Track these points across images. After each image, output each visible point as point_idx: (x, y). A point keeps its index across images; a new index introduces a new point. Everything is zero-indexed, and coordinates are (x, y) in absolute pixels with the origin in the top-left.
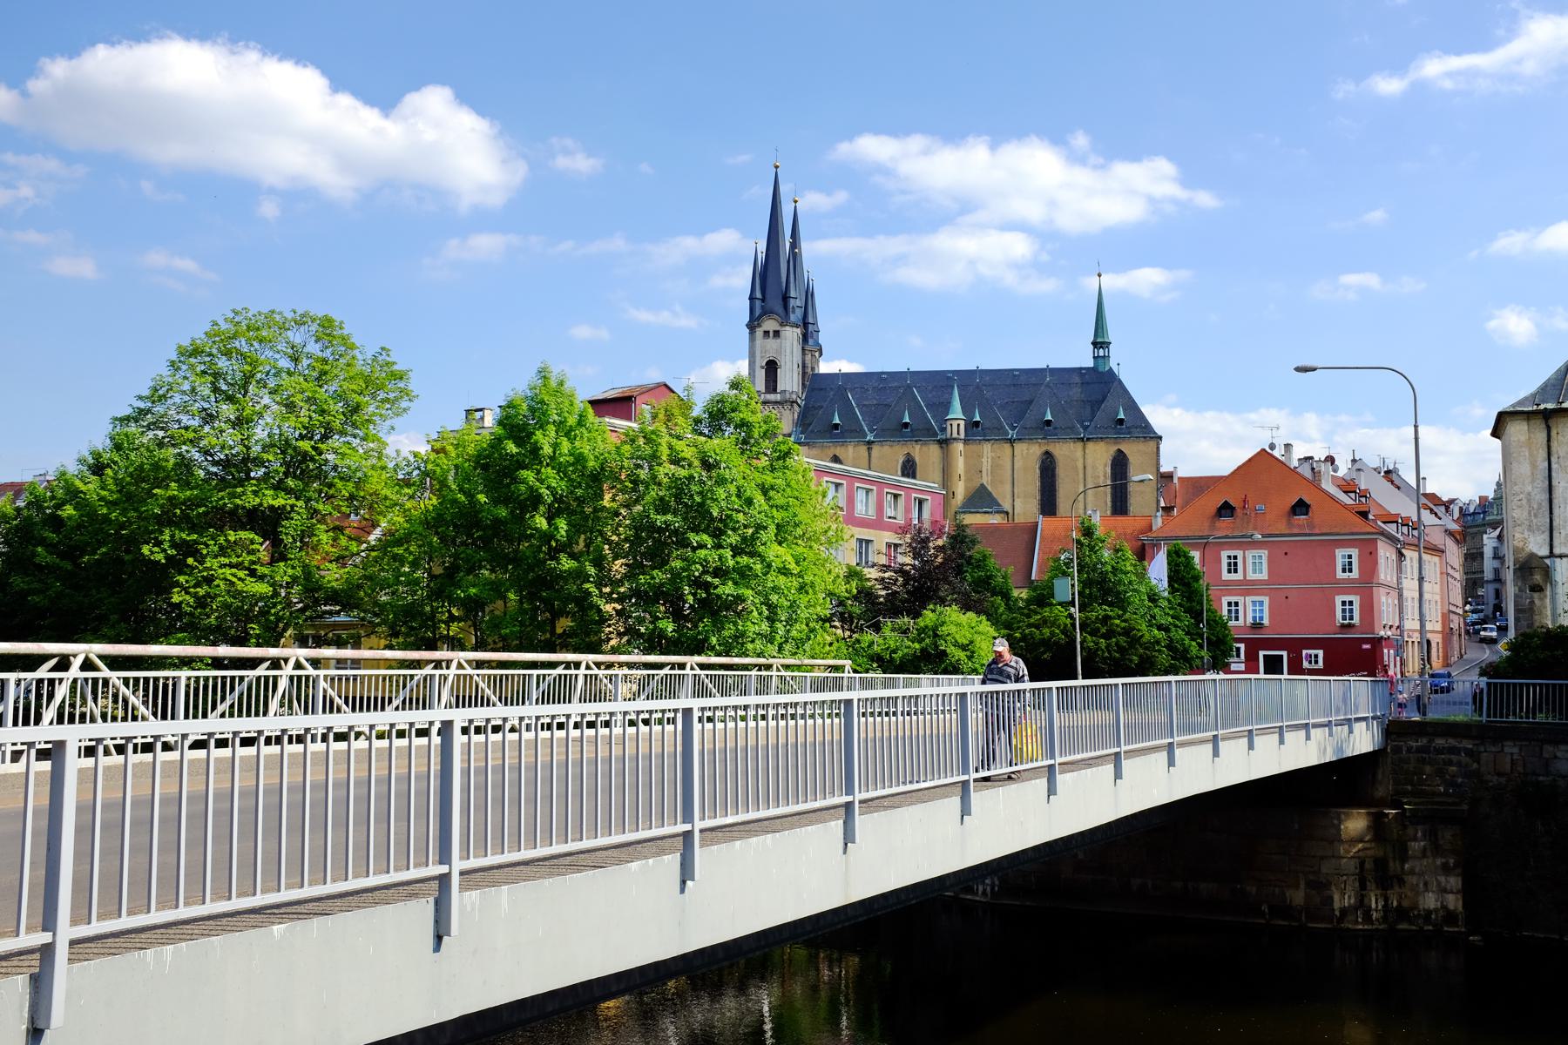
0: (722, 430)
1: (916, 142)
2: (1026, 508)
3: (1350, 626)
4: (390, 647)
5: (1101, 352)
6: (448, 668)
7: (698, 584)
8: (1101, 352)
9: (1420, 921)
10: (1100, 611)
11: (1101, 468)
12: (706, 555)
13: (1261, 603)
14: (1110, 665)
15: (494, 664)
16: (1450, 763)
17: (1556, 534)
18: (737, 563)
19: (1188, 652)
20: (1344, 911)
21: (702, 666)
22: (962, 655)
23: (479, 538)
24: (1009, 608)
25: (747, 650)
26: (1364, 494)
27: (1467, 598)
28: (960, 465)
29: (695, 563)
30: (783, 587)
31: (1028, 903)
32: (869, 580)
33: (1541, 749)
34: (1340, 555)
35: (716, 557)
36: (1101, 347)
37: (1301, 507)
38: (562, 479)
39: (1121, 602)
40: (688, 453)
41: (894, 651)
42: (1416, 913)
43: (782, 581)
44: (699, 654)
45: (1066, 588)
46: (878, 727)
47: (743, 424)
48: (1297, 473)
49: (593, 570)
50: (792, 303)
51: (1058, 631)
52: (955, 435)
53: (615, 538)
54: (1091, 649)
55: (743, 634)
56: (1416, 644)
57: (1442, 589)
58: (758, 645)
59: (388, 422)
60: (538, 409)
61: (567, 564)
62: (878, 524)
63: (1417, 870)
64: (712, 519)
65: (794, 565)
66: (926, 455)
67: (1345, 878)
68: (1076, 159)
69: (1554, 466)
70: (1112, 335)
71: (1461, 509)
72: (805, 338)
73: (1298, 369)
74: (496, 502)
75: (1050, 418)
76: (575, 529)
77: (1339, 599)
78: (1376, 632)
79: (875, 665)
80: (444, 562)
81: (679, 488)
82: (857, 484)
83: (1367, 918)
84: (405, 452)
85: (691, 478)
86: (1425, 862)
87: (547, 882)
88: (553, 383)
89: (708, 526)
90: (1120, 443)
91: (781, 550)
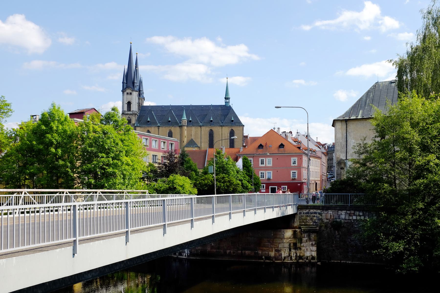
0: (109, 123)
1: (170, 38)
2: (205, 145)
3: (295, 179)
4: (6, 188)
5: (227, 101)
6: (21, 194)
7: (102, 168)
8: (227, 101)
9: (305, 259)
10: (222, 175)
11: (227, 134)
12: (104, 160)
13: (270, 173)
14: (224, 191)
15: (40, 193)
16: (314, 216)
17: (347, 153)
18: (113, 162)
19: (248, 187)
20: (285, 258)
21: (103, 193)
22: (180, 188)
23: (34, 155)
24: (196, 175)
25: (116, 187)
26: (300, 142)
27: (328, 171)
28: (185, 133)
29: (100, 162)
30: (127, 169)
31: (198, 258)
32: (155, 167)
33: (338, 212)
34: (292, 159)
35: (107, 160)
36: (227, 99)
37: (282, 146)
38: (59, 137)
39: (228, 173)
40: (99, 129)
41: (161, 188)
42: (304, 257)
43: (127, 167)
44: (102, 189)
45: (212, 169)
46: (146, 210)
47: (116, 121)
48: (281, 136)
49: (69, 165)
50: (135, 84)
51: (209, 181)
52: (184, 124)
53: (77, 155)
54: (219, 186)
55: (115, 183)
56: (313, 184)
57: (320, 168)
58: (120, 186)
59: (4, 119)
60: (51, 115)
61: (61, 162)
62: (159, 150)
63: (305, 246)
64: (106, 149)
65: (131, 162)
66: (176, 130)
67: (285, 248)
68: (218, 44)
69: (348, 135)
70: (230, 96)
71: (328, 146)
72: (139, 95)
73: (276, 107)
74: (38, 144)
75: (212, 120)
76: (64, 152)
77: (292, 172)
78: (302, 180)
79: (155, 192)
80: (23, 162)
81: (96, 140)
82: (152, 139)
83: (291, 259)
84: (9, 129)
85: (99, 137)
86: (307, 243)
87: (28, 256)
88: (56, 108)
89: (105, 151)
90: (232, 127)
91: (127, 158)
